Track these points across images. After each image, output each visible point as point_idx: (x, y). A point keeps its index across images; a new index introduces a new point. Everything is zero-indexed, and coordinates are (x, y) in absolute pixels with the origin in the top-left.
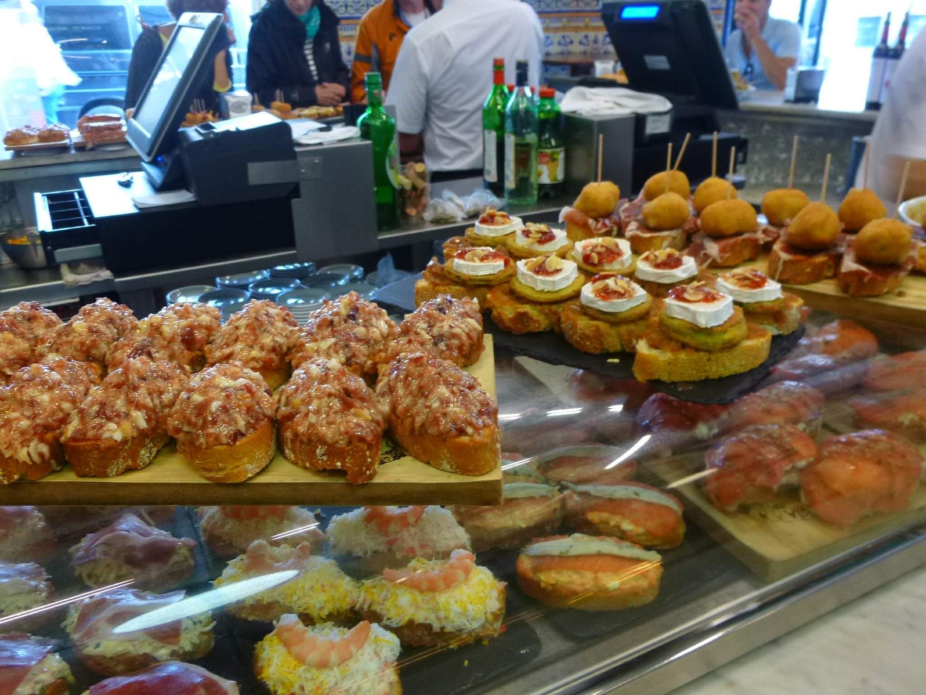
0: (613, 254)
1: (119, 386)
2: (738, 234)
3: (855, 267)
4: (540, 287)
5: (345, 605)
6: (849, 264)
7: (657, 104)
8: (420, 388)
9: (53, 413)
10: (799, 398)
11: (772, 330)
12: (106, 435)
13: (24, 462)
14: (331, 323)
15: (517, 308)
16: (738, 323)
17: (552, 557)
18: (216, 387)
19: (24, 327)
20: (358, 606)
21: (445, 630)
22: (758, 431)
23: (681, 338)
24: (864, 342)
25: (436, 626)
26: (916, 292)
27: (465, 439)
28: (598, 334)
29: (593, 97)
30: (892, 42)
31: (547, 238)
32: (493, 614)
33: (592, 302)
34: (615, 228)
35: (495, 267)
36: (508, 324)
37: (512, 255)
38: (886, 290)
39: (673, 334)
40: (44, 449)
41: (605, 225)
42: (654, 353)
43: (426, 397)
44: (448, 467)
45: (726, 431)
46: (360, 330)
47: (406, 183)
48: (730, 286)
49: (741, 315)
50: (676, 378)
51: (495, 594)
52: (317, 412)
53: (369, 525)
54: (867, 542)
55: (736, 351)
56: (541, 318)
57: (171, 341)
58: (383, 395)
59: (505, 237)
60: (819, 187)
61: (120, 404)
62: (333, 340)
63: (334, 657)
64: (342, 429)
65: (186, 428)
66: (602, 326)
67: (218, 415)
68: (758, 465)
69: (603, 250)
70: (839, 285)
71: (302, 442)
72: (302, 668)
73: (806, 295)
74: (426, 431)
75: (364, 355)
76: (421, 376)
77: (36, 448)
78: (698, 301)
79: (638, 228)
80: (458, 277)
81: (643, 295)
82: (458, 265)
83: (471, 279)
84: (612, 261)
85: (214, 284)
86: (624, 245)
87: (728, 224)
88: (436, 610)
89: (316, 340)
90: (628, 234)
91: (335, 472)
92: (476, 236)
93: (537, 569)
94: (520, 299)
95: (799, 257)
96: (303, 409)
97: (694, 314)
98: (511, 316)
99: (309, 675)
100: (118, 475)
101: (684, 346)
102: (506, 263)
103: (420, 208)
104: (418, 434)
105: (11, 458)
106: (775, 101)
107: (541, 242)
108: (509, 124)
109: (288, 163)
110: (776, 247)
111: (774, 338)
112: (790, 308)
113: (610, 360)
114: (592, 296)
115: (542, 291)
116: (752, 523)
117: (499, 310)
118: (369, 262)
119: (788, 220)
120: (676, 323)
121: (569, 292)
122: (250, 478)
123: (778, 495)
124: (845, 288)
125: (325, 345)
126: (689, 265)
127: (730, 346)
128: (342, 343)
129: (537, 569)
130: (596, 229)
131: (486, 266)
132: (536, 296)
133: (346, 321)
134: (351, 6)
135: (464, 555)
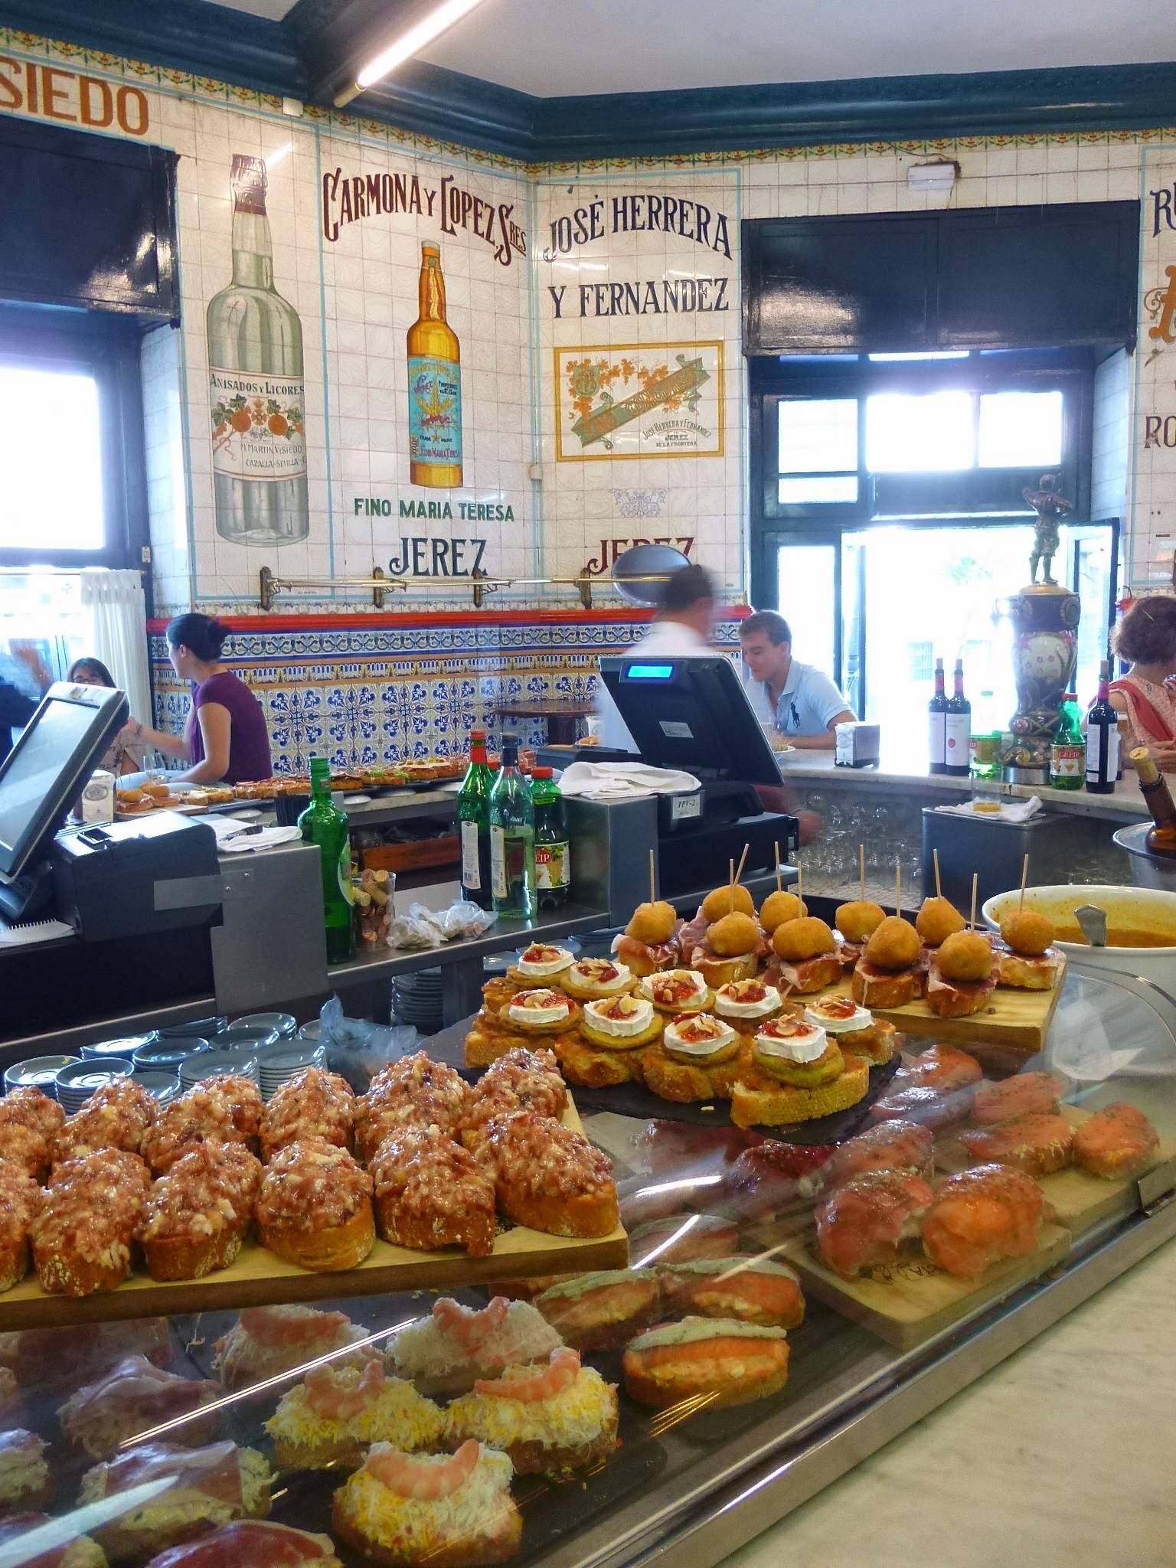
0: (686, 989)
1: (197, 1173)
2: (817, 955)
3: (942, 986)
4: (616, 1032)
5: (432, 1434)
6: (935, 983)
7: (680, 782)
8: (532, 1149)
9: (126, 1211)
10: (906, 1138)
11: (868, 1062)
12: (197, 1228)
13: (107, 1267)
14: (406, 1088)
15: (592, 1058)
16: (835, 1055)
17: (666, 1346)
18: (311, 1164)
19: (33, 1117)
20: (447, 1433)
21: (559, 1446)
22: (869, 1179)
23: (780, 1077)
24: (966, 1068)
25: (547, 1443)
26: (1005, 1008)
27: (587, 1197)
28: (688, 1082)
29: (600, 775)
30: (950, 694)
31: (609, 975)
32: (609, 1420)
33: (678, 1045)
34: (676, 956)
35: (559, 1013)
36: (583, 1077)
37: (577, 999)
38: (975, 1008)
39: (771, 1073)
40: (124, 1250)
41: (665, 953)
42: (753, 1095)
43: (539, 1158)
44: (569, 1231)
45: (833, 1181)
46: (437, 1094)
47: (364, 898)
48: (821, 1017)
49: (836, 1048)
50: (778, 1122)
51: (607, 1398)
52: (429, 1183)
53: (445, 1334)
54: (1002, 1296)
55: (837, 1085)
56: (620, 1067)
57: (223, 1120)
58: (485, 1160)
59: (557, 976)
60: (893, 871)
61: (203, 1193)
62: (412, 1107)
63: (444, 1483)
64: (460, 1198)
65: (284, 1212)
66: (693, 1071)
67: (324, 1195)
68: (875, 1216)
69: (676, 985)
70: (928, 1006)
71: (413, 1217)
72: (409, 1502)
73: (896, 1019)
74: (544, 1193)
75: (446, 1122)
76: (528, 1136)
77: (117, 1251)
78: (792, 1036)
79: (705, 956)
80: (518, 1027)
81: (731, 1034)
82: (517, 1013)
83: (533, 1028)
84: (687, 997)
85: (79, 1055)
86: (698, 978)
87: (805, 948)
88: (545, 1422)
89: (392, 1109)
90: (694, 963)
91: (455, 1248)
92: (520, 976)
93: (648, 1366)
94: (595, 1047)
95: (884, 979)
96: (412, 1181)
97: (790, 1049)
98: (586, 1067)
99: (416, 1511)
100: (206, 1274)
101: (783, 1085)
102: (571, 1007)
103: (382, 930)
104: (534, 1198)
105: (93, 1263)
106: (823, 765)
107: (603, 980)
108: (494, 814)
109: (211, 878)
110: (858, 968)
111: (872, 1069)
112: (882, 1035)
113: (703, 1109)
114: (677, 1038)
115: (619, 1036)
116: (877, 1287)
117: (571, 1061)
118: (306, 1011)
119: (866, 937)
120: (772, 1061)
121: (649, 1035)
122: (360, 1264)
123: (899, 1251)
124: (935, 1008)
125: (402, 1113)
126: (773, 998)
127: (830, 1081)
128: (422, 1109)
129: (648, 1366)
130: (656, 959)
131: (549, 1013)
132: (613, 1043)
133: (421, 1085)
134: (239, 645)
135: (565, 1354)
